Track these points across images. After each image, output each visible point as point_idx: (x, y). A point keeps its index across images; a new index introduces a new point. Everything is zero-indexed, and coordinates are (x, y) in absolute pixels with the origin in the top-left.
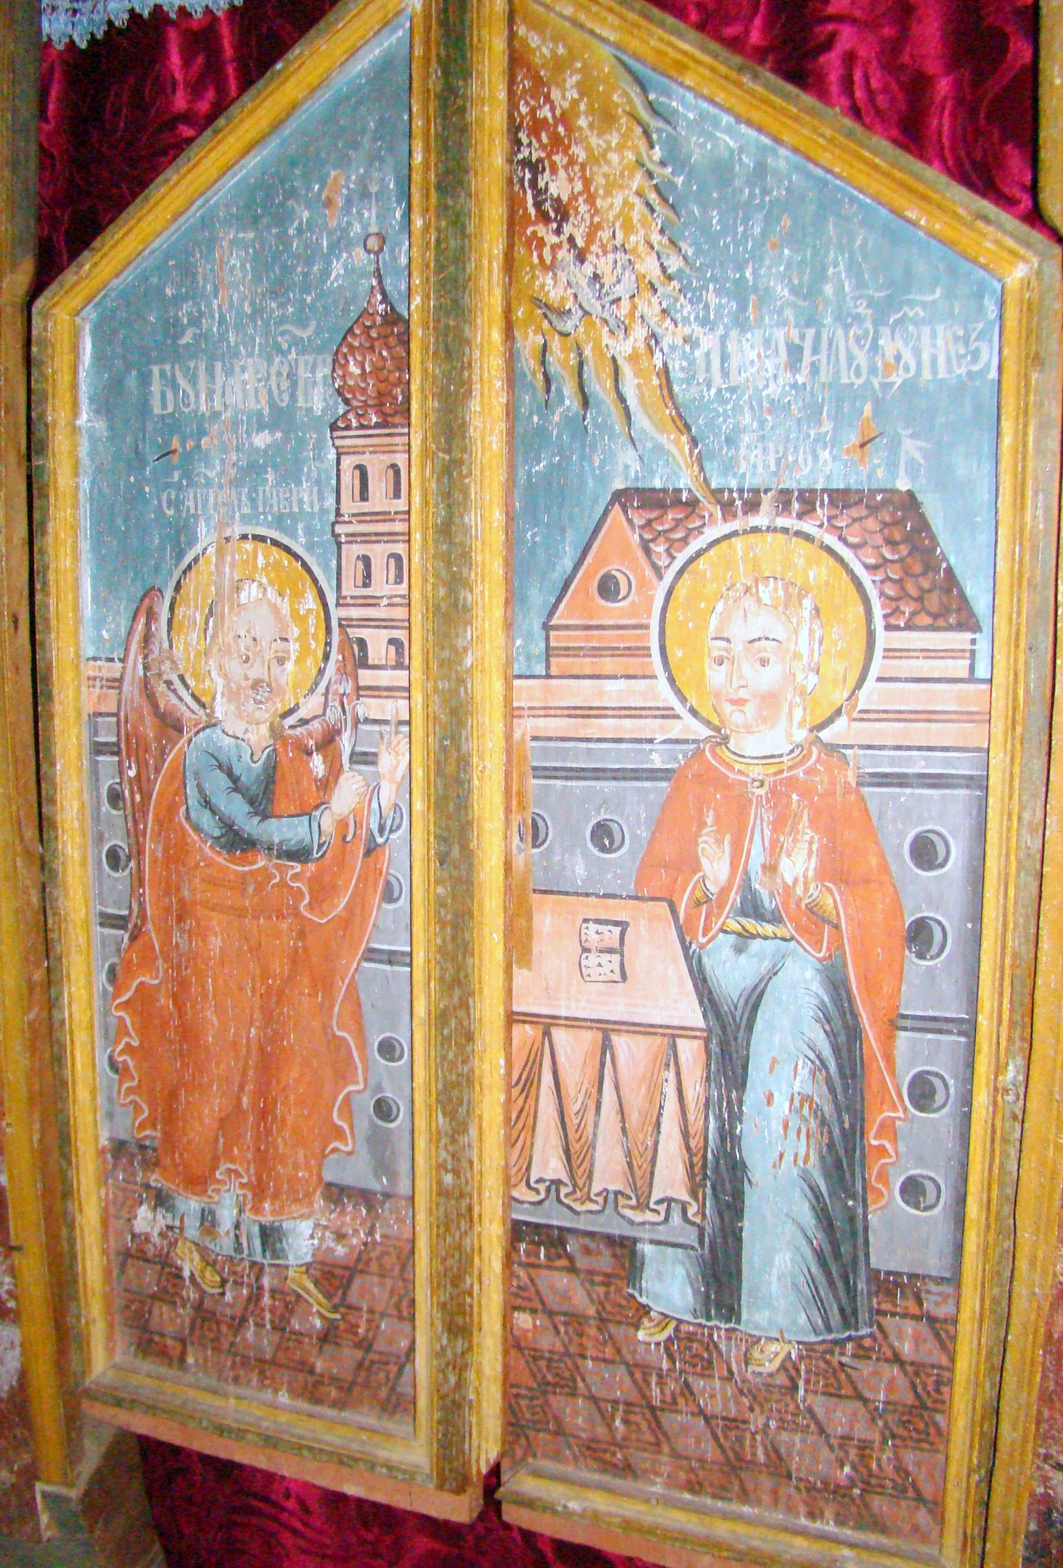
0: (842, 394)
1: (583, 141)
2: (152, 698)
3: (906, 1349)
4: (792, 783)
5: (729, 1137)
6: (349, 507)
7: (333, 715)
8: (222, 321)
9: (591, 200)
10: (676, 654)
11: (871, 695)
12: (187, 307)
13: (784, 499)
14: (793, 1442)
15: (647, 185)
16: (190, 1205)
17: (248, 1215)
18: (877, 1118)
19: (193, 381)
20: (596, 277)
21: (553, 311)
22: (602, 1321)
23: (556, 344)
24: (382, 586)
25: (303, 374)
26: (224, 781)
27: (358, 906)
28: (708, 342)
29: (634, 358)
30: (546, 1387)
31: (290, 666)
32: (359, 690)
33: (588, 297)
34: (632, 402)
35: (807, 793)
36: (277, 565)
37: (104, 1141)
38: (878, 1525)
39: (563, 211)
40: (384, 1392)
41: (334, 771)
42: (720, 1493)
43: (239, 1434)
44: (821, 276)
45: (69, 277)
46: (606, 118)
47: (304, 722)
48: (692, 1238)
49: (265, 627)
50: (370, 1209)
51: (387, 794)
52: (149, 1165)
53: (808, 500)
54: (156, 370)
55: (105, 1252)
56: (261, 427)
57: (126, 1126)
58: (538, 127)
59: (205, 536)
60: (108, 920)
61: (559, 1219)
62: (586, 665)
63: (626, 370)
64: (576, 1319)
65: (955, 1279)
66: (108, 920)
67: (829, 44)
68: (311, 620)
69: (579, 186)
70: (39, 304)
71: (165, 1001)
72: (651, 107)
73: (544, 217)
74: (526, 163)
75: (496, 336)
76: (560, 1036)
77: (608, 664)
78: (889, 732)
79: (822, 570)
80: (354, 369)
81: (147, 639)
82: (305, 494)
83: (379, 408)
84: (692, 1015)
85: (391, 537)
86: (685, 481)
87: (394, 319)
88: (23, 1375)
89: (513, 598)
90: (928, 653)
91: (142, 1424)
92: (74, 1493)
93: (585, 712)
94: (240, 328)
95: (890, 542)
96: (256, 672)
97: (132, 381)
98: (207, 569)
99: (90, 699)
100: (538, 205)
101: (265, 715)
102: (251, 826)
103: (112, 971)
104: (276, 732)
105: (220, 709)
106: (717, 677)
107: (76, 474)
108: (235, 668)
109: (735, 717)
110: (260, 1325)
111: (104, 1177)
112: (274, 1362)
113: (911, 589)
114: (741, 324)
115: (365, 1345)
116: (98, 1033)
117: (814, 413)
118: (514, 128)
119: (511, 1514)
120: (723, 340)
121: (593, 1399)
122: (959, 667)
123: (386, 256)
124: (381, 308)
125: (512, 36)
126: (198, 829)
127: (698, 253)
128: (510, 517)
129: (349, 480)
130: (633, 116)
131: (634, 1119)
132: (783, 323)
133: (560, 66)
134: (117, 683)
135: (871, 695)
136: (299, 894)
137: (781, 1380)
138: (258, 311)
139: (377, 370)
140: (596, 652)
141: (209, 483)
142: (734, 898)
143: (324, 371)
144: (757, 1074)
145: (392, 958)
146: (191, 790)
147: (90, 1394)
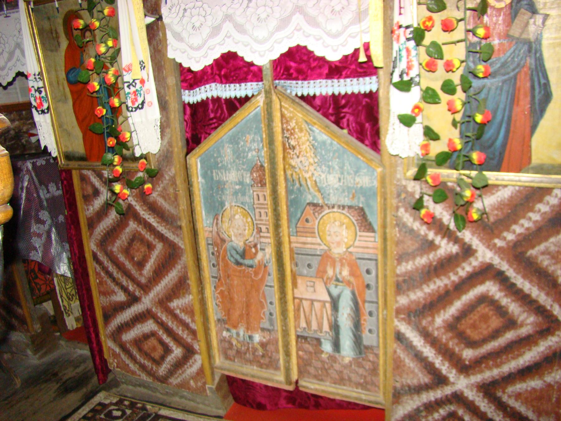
0: (349, 188)
1: (297, 134)
2: (219, 235)
3: (371, 359)
4: (343, 258)
5: (336, 321)
6: (256, 202)
7: (256, 241)
8: (227, 162)
9: (299, 146)
10: (321, 234)
11: (357, 243)
12: (219, 159)
13: (339, 207)
14: (353, 376)
15: (310, 144)
16: (234, 331)
17: (246, 333)
18: (363, 318)
19: (222, 174)
20: (301, 162)
21: (293, 167)
22: (315, 353)
23: (294, 174)
24: (264, 217)
25: (245, 175)
26: (235, 252)
27: (263, 277)
28: (323, 176)
29: (309, 178)
30: (305, 365)
31: (247, 231)
32: (261, 237)
33: (300, 165)
34: (310, 186)
35: (346, 260)
36: (242, 212)
37: (216, 319)
38: (368, 390)
39: (294, 148)
40: (275, 366)
41: (257, 252)
42: (340, 384)
43: (247, 375)
44: (344, 165)
45: (194, 152)
46: (301, 130)
47: (250, 242)
48: (330, 338)
49: (241, 223)
50: (270, 332)
51: (268, 256)
52: (225, 324)
53: (344, 207)
54: (214, 171)
55: (217, 340)
56: (237, 184)
57: (220, 316)
58: (288, 130)
59: (227, 205)
60: (213, 277)
61: (305, 334)
62: (304, 234)
63: (308, 180)
64: (310, 353)
65: (378, 347)
66: (213, 277)
67: (344, 117)
68: (250, 223)
69: (297, 143)
70: (188, 157)
71: (226, 293)
72: (310, 129)
73: (290, 148)
74: (286, 137)
75: (282, 173)
76: (304, 302)
77: (308, 235)
78: (360, 250)
79: (346, 221)
80: (255, 175)
81: (217, 224)
82: (247, 199)
83: (260, 183)
84: (327, 298)
85: (264, 208)
86: (320, 202)
87: (262, 166)
88: (202, 365)
89: (289, 221)
90: (367, 237)
91: (227, 373)
92: (214, 387)
93: (304, 243)
94: (231, 164)
95: (359, 216)
96: (240, 232)
97: (209, 172)
98: (228, 211)
99: (206, 234)
100: (289, 146)
101: (242, 240)
102: (241, 261)
103: (215, 287)
104: (245, 244)
105: (233, 238)
106: (328, 238)
107: (199, 191)
108: (236, 231)
109: (332, 246)
110: (249, 354)
111: (216, 326)
112: (253, 361)
113: (363, 224)
114: (329, 173)
115: (270, 357)
116: (213, 299)
117: (343, 191)
118: (283, 130)
119: (301, 389)
120: (326, 176)
121: (315, 367)
122: (372, 239)
123: (259, 154)
124: (259, 164)
125: (281, 111)
126: (230, 261)
127: (321, 158)
128: (287, 207)
129: (256, 197)
130: (306, 130)
131: (319, 317)
132: (337, 173)
133: (292, 118)
134: (211, 232)
135: (357, 243)
136: (251, 274)
137: (349, 364)
138: (234, 162)
139: (259, 176)
140: (306, 232)
141: (227, 194)
142: (334, 278)
143: (249, 175)
144: (341, 309)
145: (271, 286)
146: (228, 253)
147: (216, 368)
